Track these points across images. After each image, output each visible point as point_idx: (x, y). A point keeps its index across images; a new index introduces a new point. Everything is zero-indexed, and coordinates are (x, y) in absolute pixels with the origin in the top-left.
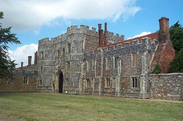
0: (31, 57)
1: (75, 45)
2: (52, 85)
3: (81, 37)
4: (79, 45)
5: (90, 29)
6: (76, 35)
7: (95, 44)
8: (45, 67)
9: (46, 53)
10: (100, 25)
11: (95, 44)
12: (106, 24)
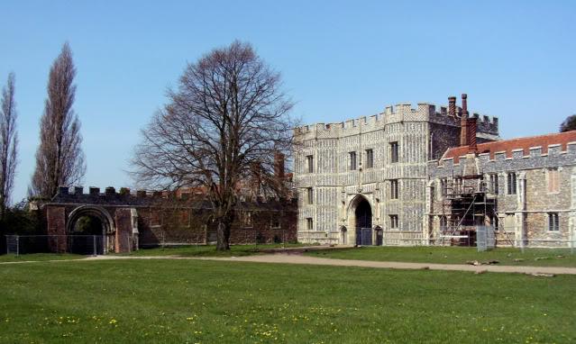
2: (338, 229)
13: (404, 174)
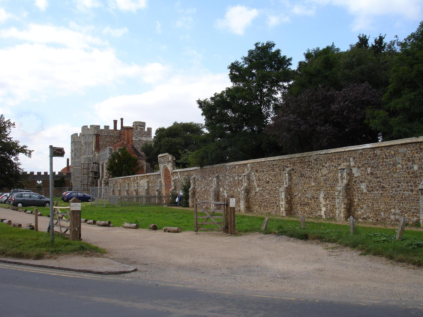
0: (69, 159)
1: (85, 147)
3: (91, 138)
4: (90, 146)
5: (102, 128)
6: (87, 136)
7: (108, 144)
8: (74, 167)
9: (76, 152)
10: (115, 122)
11: (108, 144)
12: (122, 119)
13: (84, 161)
